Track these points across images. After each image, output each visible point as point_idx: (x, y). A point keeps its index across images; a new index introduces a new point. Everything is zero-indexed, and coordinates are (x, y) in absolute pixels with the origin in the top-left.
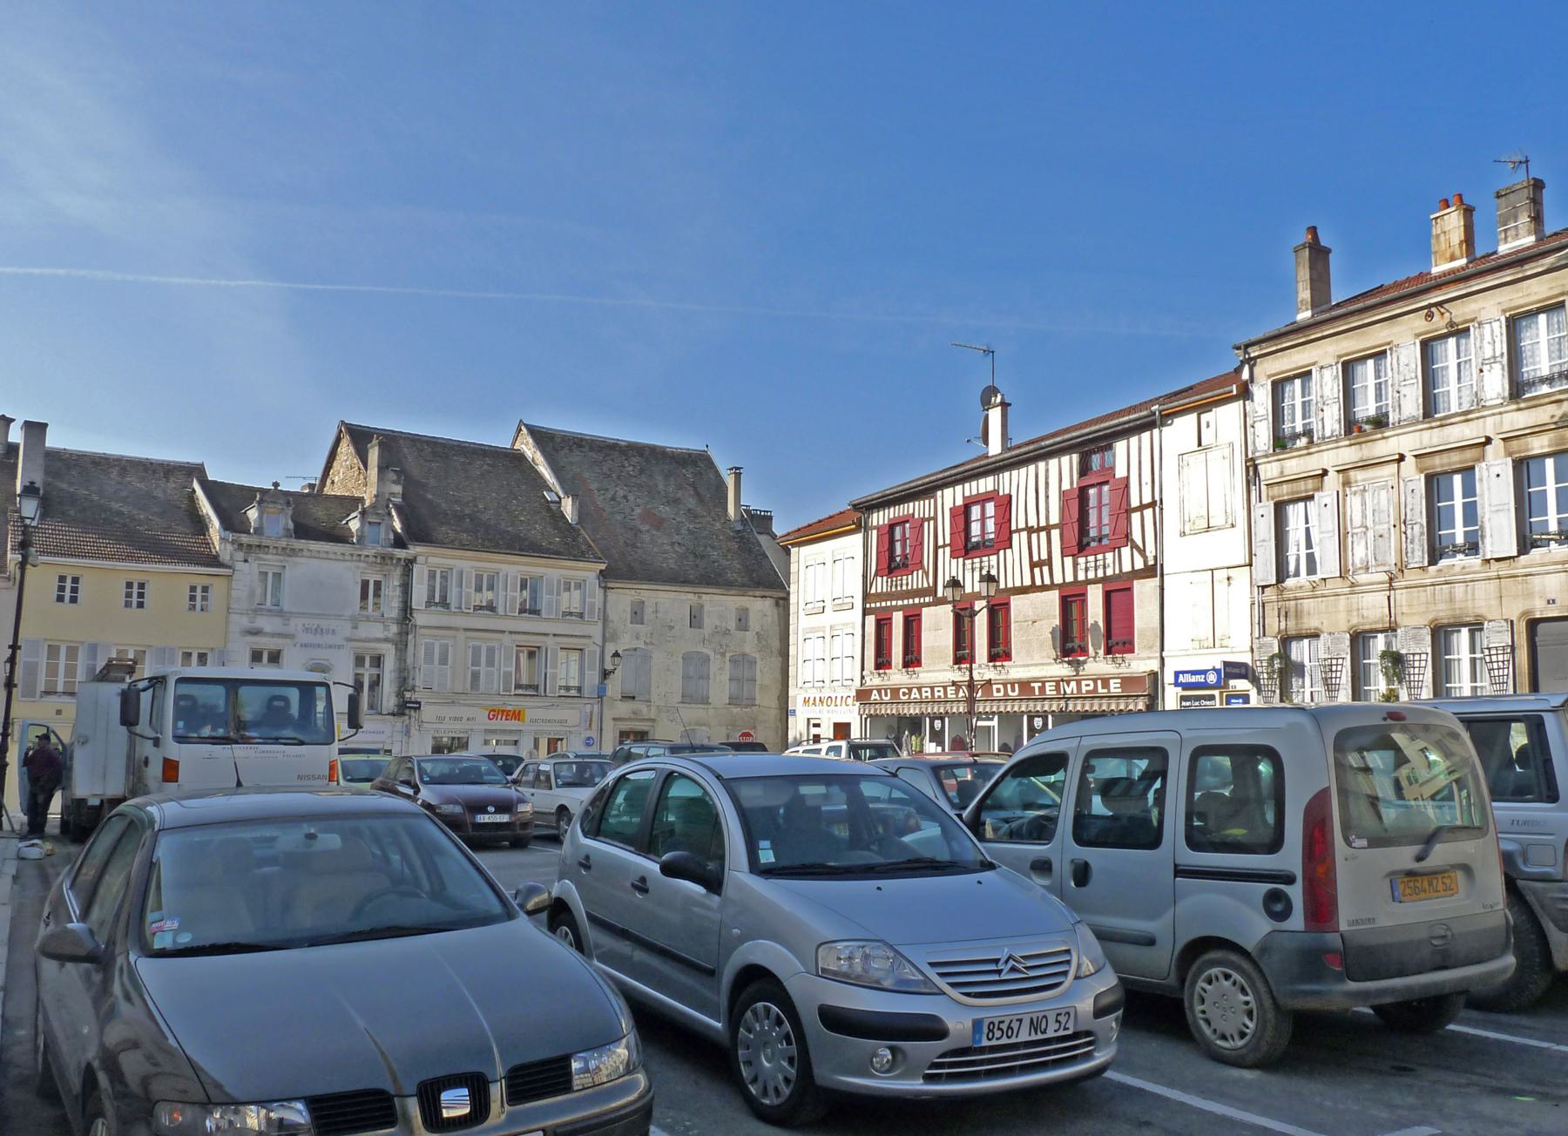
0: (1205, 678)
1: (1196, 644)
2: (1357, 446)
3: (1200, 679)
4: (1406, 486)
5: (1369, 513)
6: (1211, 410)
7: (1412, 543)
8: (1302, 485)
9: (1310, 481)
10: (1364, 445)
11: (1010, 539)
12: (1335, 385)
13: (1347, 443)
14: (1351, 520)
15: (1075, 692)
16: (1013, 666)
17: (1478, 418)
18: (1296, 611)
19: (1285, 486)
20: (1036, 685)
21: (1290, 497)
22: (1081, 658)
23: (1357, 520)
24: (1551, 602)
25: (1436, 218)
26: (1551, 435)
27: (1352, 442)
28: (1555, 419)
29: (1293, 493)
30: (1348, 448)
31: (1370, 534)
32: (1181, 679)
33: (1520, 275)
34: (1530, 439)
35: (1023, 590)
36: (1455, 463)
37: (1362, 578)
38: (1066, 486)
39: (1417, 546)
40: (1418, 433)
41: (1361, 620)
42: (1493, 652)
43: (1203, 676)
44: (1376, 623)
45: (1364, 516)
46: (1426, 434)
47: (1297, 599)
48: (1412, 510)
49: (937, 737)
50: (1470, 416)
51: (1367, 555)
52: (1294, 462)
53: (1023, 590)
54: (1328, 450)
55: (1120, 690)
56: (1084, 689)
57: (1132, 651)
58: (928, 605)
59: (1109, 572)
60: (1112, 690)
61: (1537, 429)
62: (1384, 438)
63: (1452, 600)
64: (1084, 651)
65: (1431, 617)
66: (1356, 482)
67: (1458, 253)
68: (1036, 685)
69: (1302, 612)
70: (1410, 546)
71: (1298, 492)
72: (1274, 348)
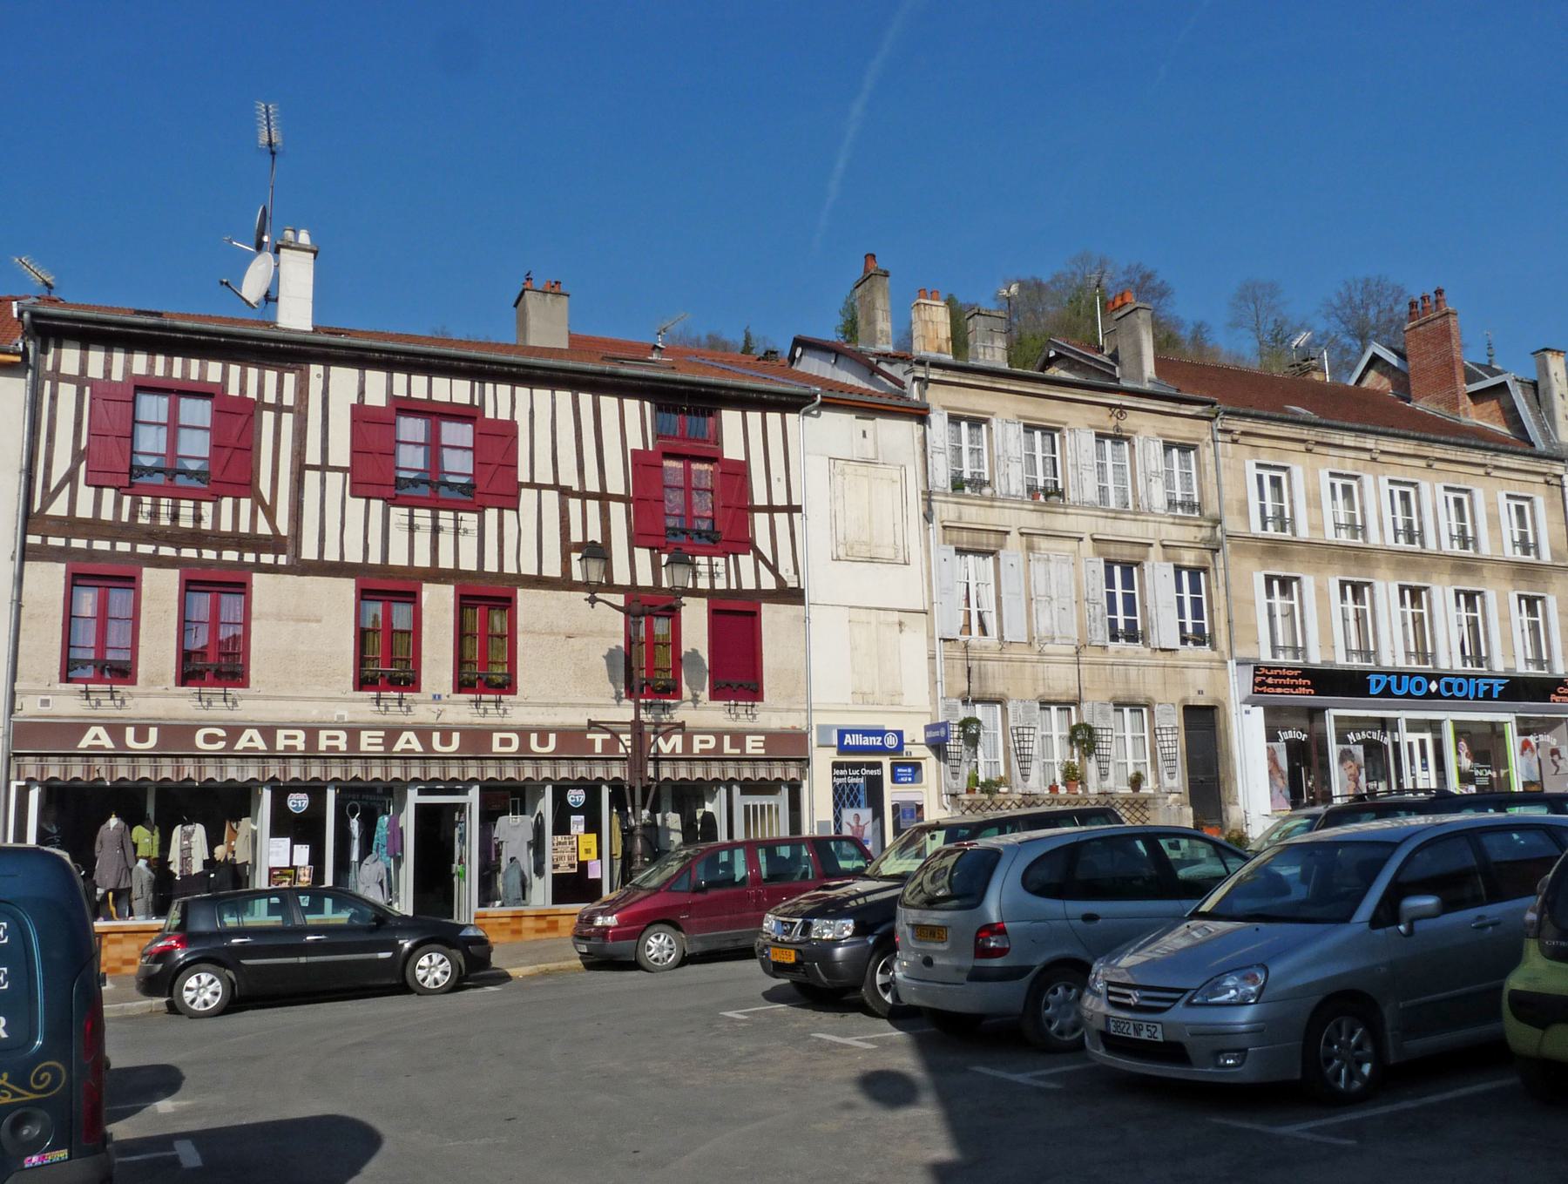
0: (882, 741)
1: (859, 698)
2: (1039, 514)
3: (875, 741)
4: (1086, 566)
5: (1053, 586)
6: (873, 419)
7: (1095, 622)
8: (984, 537)
9: (992, 536)
10: (1045, 515)
11: (517, 497)
12: (1018, 445)
13: (1032, 507)
14: (1035, 586)
15: (679, 750)
16: (519, 704)
17: (1143, 521)
18: (980, 673)
19: (965, 534)
20: (598, 739)
21: (970, 547)
22: (672, 701)
23: (1041, 589)
24: (1200, 692)
25: (925, 304)
26: (1196, 552)
27: (1037, 508)
28: (1198, 540)
29: (974, 544)
30: (1030, 513)
31: (1055, 604)
32: (848, 740)
33: (1175, 411)
34: (1182, 551)
35: (540, 582)
36: (1126, 555)
37: (1049, 648)
38: (635, 442)
39: (1099, 626)
40: (1094, 518)
41: (1047, 690)
42: (1164, 732)
43: (880, 739)
44: (1061, 694)
45: (1048, 586)
46: (1101, 522)
47: (980, 660)
48: (1093, 590)
49: (284, 824)
50: (1139, 517)
51: (1052, 625)
52: (974, 510)
53: (540, 582)
54: (1010, 508)
55: (763, 751)
56: (697, 748)
57: (244, 683)
58: (273, 569)
59: (720, 584)
60: (749, 750)
61: (1049, 533)
62: (1065, 513)
63: (1127, 681)
64: (675, 692)
65: (1111, 694)
66: (1039, 549)
67: (944, 347)
68: (598, 739)
69: (986, 674)
70: (1093, 624)
71: (978, 544)
72: (956, 380)
